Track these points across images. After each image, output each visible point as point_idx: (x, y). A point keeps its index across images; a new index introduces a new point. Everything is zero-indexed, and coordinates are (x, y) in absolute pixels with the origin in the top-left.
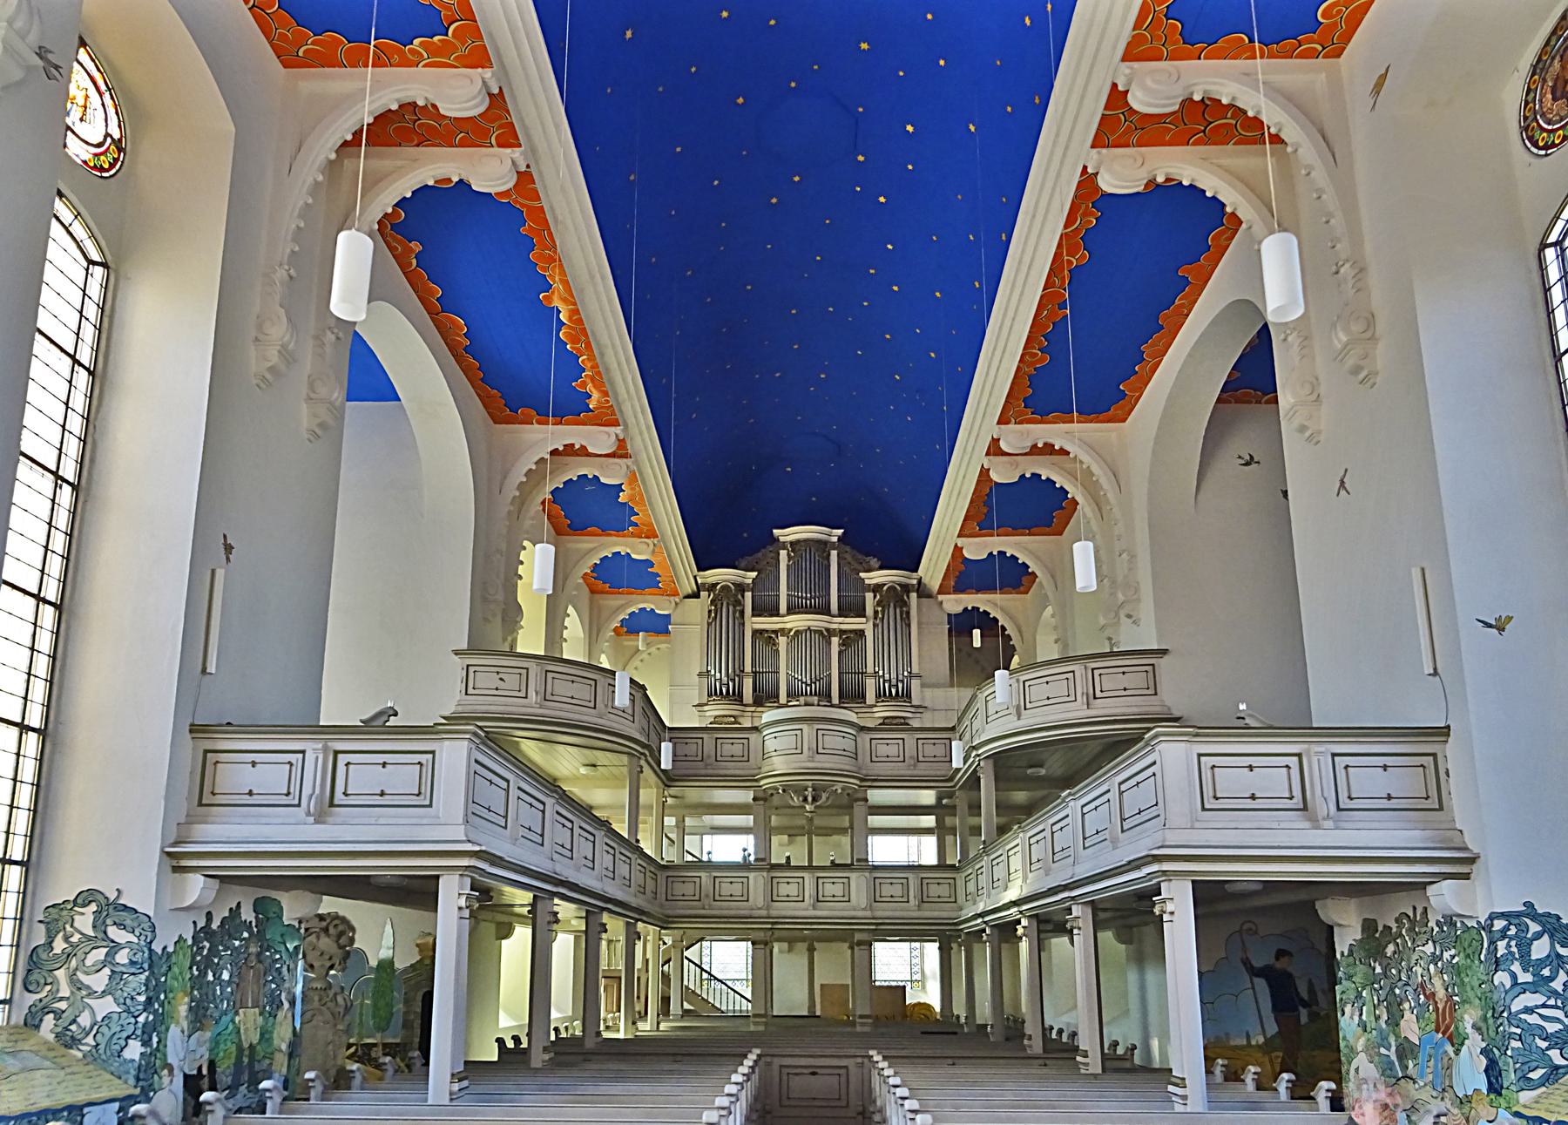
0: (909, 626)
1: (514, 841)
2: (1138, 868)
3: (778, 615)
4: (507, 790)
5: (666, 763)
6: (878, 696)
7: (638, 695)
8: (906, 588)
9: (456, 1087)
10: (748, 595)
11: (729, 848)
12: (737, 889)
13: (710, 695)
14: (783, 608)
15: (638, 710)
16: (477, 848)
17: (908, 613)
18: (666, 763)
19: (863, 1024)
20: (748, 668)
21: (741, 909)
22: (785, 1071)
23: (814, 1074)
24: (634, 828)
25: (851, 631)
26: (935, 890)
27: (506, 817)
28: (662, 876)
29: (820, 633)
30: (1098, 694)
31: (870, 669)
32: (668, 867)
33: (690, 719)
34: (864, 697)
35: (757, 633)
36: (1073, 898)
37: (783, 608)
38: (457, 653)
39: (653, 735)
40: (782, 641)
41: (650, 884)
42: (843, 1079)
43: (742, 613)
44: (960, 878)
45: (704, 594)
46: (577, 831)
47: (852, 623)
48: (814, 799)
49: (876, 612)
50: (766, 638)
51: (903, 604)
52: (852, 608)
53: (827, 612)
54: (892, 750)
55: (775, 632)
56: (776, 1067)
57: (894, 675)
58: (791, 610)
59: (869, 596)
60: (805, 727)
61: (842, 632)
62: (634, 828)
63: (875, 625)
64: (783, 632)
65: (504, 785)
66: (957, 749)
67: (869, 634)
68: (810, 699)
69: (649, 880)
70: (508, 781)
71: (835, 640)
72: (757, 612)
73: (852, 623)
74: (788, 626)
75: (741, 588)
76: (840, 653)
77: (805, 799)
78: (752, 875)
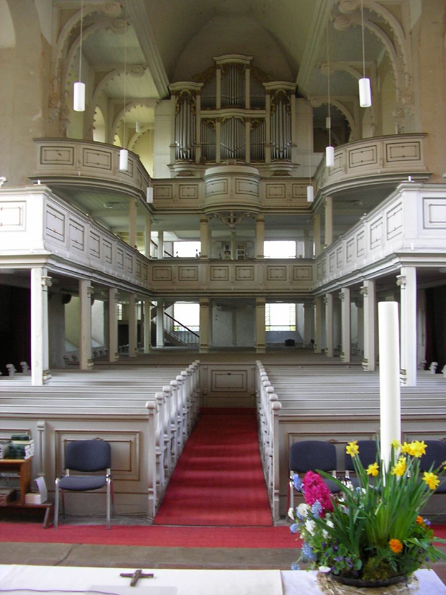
0: (290, 115)
1: (68, 248)
2: (390, 260)
3: (215, 109)
4: (64, 221)
5: (150, 199)
6: (272, 157)
7: (135, 161)
8: (289, 92)
9: (45, 377)
10: (198, 97)
11: (188, 249)
12: (191, 274)
13: (177, 158)
14: (218, 104)
15: (135, 170)
16: (50, 253)
17: (290, 107)
18: (150, 199)
19: (260, 349)
20: (198, 141)
21: (194, 286)
22: (214, 373)
23: (229, 374)
24: (167, 318)
25: (257, 119)
26: (300, 273)
27: (63, 235)
28: (150, 266)
29: (240, 119)
30: (389, 159)
31: (268, 141)
32: (154, 261)
33: (166, 174)
34: (264, 158)
35: (204, 120)
36: (364, 277)
37: (218, 104)
38: (36, 140)
39: (144, 183)
40: (218, 125)
41: (143, 270)
42: (245, 376)
43: (195, 108)
44: (315, 266)
45: (173, 97)
46: (68, 222)
47: (209, 114)
48: (235, 220)
49: (271, 107)
50: (209, 124)
51: (286, 101)
52: (258, 104)
53: (242, 106)
54: (278, 191)
55: (214, 119)
56: (209, 371)
57: (281, 145)
58: (224, 106)
59: (268, 97)
60: (229, 178)
61: (252, 119)
62: (167, 318)
63: (271, 115)
64: (219, 119)
65: (62, 217)
66: (310, 191)
67: (267, 120)
68: (231, 161)
69: (142, 268)
70: (111, 244)
71: (248, 125)
72: (204, 107)
73: (257, 114)
74: (222, 115)
75: (194, 93)
76: (251, 131)
77: (229, 221)
78: (200, 266)
